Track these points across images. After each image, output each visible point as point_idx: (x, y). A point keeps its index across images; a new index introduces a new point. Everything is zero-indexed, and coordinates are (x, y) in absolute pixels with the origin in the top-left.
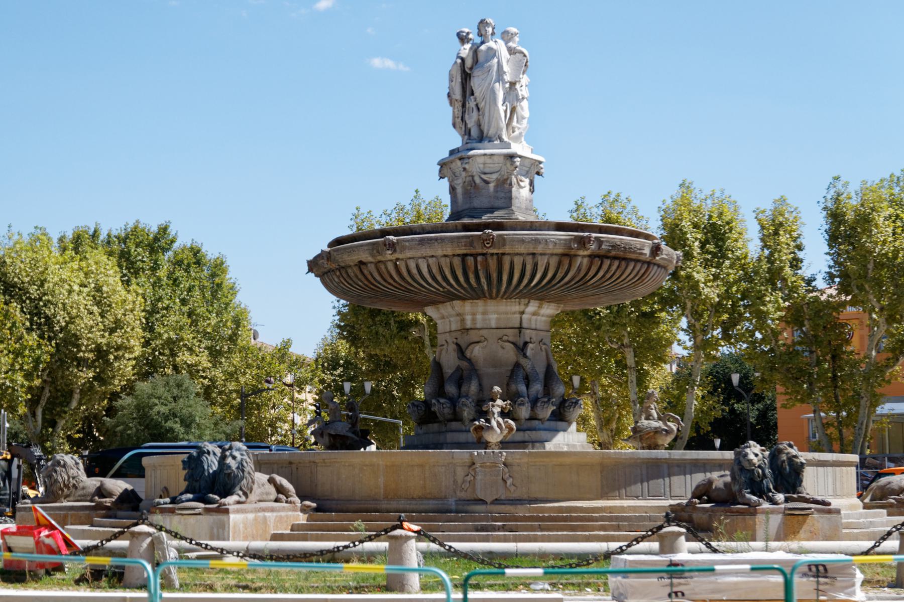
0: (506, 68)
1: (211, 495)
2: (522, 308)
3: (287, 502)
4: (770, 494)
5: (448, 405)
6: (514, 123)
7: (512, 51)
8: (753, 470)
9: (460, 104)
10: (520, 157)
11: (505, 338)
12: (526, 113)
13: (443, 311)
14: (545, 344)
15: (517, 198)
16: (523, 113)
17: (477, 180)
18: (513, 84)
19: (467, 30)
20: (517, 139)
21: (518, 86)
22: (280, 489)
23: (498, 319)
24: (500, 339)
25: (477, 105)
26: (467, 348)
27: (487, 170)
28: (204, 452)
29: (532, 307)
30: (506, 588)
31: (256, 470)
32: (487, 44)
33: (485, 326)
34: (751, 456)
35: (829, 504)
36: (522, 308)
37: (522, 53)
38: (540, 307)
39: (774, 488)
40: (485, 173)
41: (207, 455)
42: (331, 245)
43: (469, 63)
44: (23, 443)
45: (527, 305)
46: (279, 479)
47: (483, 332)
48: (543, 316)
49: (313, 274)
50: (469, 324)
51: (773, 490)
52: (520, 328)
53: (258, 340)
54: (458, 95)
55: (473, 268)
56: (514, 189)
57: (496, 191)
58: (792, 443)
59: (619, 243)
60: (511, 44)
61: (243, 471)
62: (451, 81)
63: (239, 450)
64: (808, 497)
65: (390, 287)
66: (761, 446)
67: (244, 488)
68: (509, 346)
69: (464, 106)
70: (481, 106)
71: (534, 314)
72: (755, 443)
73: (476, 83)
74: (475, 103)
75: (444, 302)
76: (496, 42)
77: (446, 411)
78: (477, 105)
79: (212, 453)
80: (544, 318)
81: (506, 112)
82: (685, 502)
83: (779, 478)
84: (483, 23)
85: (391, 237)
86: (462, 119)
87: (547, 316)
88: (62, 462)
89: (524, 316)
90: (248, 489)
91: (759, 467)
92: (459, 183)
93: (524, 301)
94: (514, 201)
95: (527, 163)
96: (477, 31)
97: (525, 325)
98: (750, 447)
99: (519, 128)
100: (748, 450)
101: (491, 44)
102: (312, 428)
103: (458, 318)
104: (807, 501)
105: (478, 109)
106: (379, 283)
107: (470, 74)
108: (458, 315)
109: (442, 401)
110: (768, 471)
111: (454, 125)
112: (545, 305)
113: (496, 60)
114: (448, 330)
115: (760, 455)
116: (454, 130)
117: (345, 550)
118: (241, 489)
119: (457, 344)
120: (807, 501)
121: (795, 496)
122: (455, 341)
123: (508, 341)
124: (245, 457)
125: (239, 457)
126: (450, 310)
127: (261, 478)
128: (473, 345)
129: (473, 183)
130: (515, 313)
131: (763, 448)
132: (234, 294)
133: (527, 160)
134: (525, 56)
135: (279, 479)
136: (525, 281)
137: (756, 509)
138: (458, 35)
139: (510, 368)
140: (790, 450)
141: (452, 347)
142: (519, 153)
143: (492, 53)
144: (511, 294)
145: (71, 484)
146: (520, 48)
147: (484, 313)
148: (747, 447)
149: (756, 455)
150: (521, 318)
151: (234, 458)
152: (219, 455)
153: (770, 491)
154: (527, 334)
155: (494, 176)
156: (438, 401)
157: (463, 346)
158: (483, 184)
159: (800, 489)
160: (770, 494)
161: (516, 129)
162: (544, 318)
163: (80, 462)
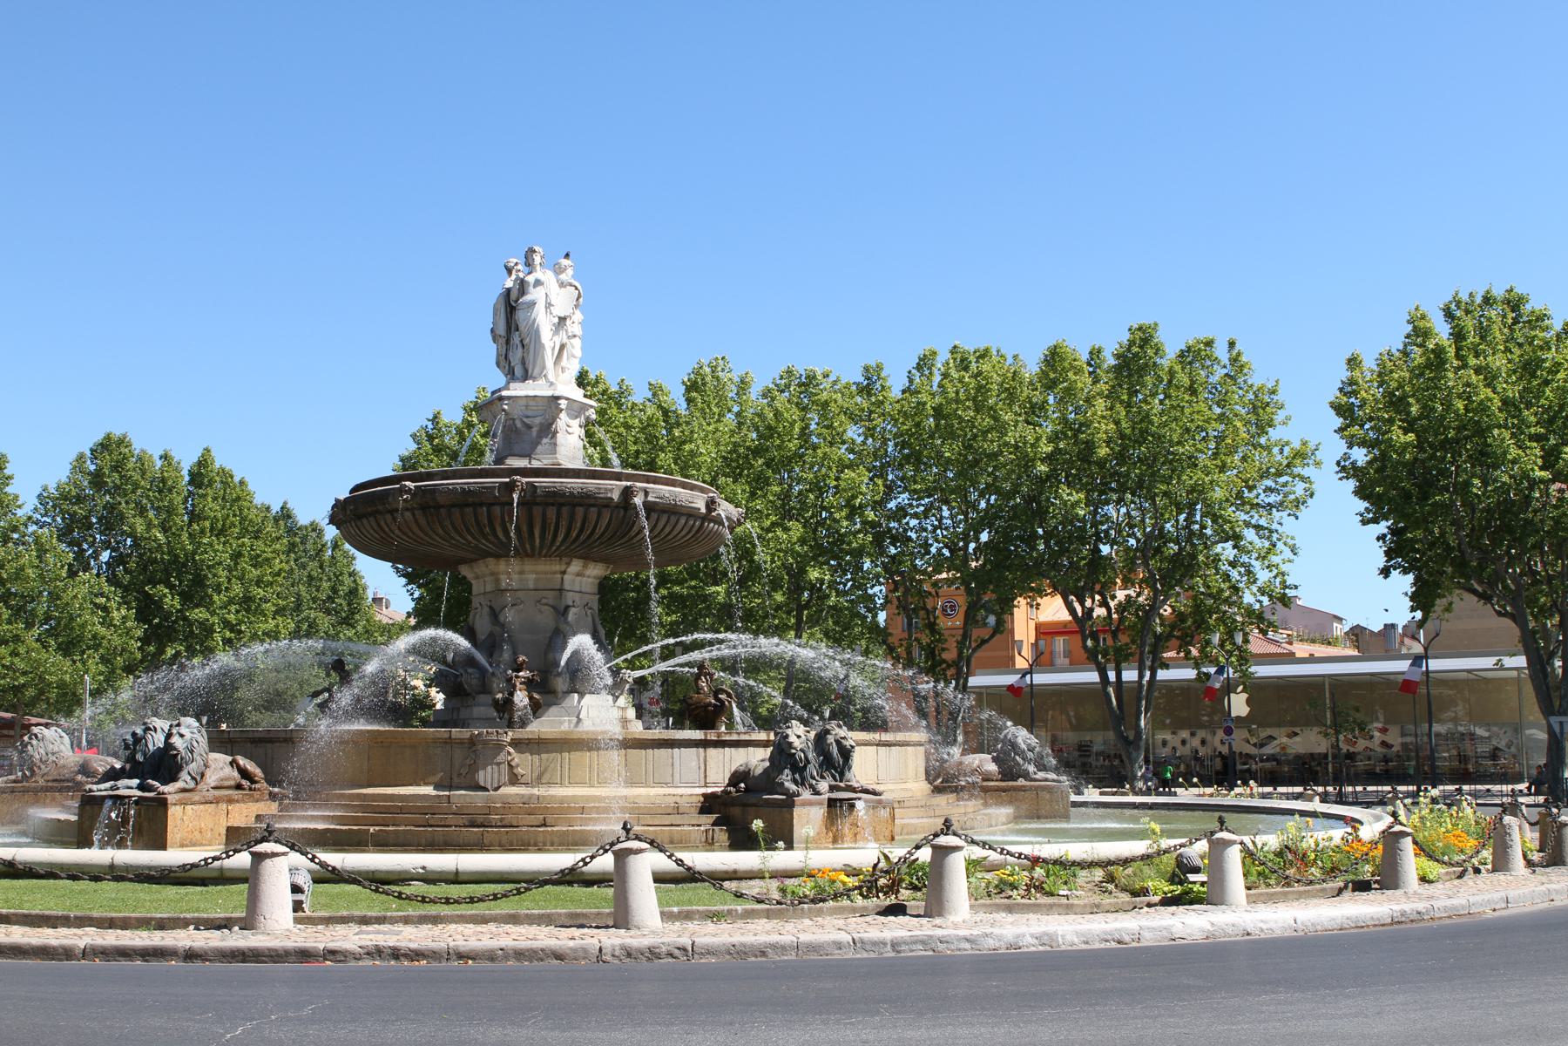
1: (150, 781)
3: (250, 789)
4: (814, 782)
5: (477, 676)
8: (795, 754)
9: (504, 340)
10: (567, 399)
11: (544, 601)
13: (476, 570)
14: (590, 608)
17: (519, 424)
18: (562, 320)
21: (568, 322)
22: (244, 773)
23: (536, 580)
25: (521, 341)
27: (530, 413)
29: (576, 566)
31: (212, 750)
33: (522, 587)
34: (792, 739)
38: (585, 566)
40: (527, 417)
41: (153, 733)
42: (351, 492)
43: (514, 295)
45: (568, 564)
46: (242, 761)
47: (520, 594)
48: (589, 577)
52: (561, 590)
54: (502, 330)
55: (499, 520)
59: (667, 495)
60: (563, 277)
61: (192, 752)
62: (495, 314)
63: (189, 727)
64: (856, 785)
65: (405, 537)
66: (805, 726)
68: (547, 610)
69: (508, 342)
70: (525, 343)
71: (578, 575)
72: (798, 723)
73: (520, 315)
75: (476, 560)
77: (474, 682)
78: (521, 341)
79: (159, 730)
80: (590, 580)
81: (553, 349)
82: (720, 789)
85: (407, 483)
86: (506, 358)
87: (595, 577)
89: (566, 577)
91: (802, 750)
93: (565, 560)
94: (558, 448)
95: (575, 405)
97: (567, 587)
100: (789, 731)
102: (63, 721)
103: (492, 578)
104: (854, 790)
105: (523, 346)
108: (492, 574)
109: (470, 670)
110: (811, 756)
111: (498, 364)
112: (591, 566)
115: (803, 737)
119: (491, 607)
120: (854, 790)
121: (842, 785)
123: (546, 604)
124: (197, 736)
125: (188, 736)
126: (484, 569)
127: (220, 760)
130: (555, 573)
132: (1412, 606)
133: (575, 404)
134: (576, 289)
135: (242, 761)
138: (506, 267)
139: (549, 635)
140: (837, 730)
141: (486, 610)
144: (550, 548)
147: (521, 573)
148: (788, 727)
149: (799, 737)
151: (182, 736)
153: (813, 778)
154: (569, 598)
155: (538, 421)
156: (466, 671)
158: (524, 429)
159: (848, 775)
162: (590, 580)
163: (63, 734)
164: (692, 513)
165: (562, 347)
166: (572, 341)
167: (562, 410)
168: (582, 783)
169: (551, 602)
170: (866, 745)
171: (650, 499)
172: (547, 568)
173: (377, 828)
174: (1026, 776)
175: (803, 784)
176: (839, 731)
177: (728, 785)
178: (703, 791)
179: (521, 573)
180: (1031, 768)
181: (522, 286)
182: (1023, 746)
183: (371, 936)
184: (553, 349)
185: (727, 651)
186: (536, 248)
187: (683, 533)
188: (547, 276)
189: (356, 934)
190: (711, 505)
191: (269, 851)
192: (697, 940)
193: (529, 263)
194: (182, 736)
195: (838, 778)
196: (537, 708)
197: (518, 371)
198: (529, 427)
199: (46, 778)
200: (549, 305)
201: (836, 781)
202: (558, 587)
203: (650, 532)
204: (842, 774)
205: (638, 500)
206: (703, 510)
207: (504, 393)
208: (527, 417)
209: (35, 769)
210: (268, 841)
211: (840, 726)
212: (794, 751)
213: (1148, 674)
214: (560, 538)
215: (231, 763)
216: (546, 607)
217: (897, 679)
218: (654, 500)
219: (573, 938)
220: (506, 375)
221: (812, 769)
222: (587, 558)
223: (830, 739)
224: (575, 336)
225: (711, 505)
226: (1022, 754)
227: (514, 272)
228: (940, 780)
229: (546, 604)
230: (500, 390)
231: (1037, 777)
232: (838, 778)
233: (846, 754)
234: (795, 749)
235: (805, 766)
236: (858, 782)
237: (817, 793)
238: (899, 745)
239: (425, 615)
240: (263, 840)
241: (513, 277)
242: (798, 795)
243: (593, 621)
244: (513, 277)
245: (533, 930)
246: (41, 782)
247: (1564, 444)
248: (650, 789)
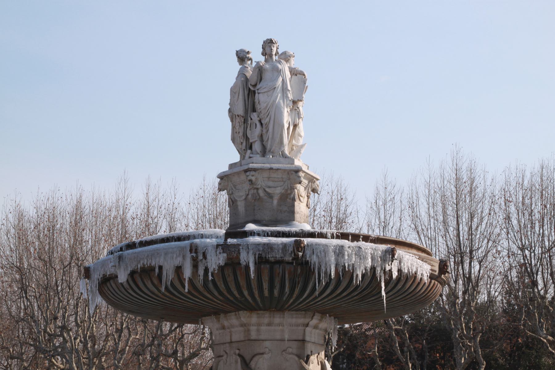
2: (306, 321)
11: (290, 350)
15: (298, 213)
24: (284, 351)
25: (260, 121)
26: (251, 360)
36: (306, 321)
40: (269, 187)
44: (535, 328)
50: (253, 335)
52: (303, 341)
54: (240, 111)
56: (296, 203)
57: (279, 205)
69: (245, 121)
73: (262, 99)
74: (258, 119)
84: (269, 43)
92: (240, 195)
96: (262, 50)
97: (307, 338)
105: (262, 124)
106: (160, 298)
107: (254, 92)
108: (243, 325)
111: (233, 140)
114: (229, 341)
116: (233, 144)
122: (237, 352)
123: (292, 354)
128: (257, 357)
129: (257, 198)
136: (328, 291)
138: (238, 53)
150: (304, 330)
157: (247, 358)
158: (266, 198)
169: (295, 351)
172: (294, 321)
179: (259, 325)
198: (270, 196)
200: (284, 89)
202: (301, 338)
208: (269, 187)
213: (470, 237)
214: (328, 291)
216: (291, 356)
229: (292, 354)
247: (121, 369)
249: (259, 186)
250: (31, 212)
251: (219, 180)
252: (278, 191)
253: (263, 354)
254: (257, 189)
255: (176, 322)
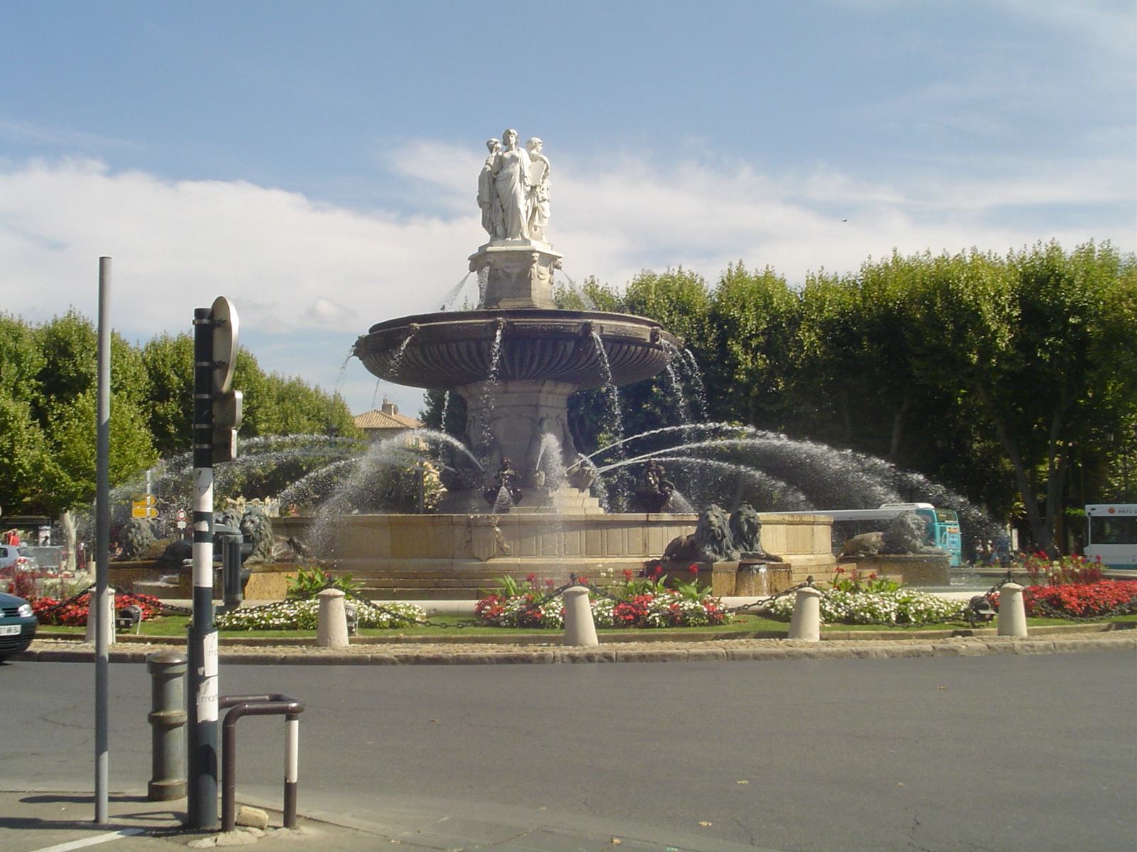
0: (527, 173)
4: (729, 551)
6: (536, 222)
7: (533, 158)
8: (713, 530)
12: (547, 213)
14: (561, 420)
16: (544, 214)
17: (501, 274)
18: (533, 188)
19: (495, 140)
20: (539, 238)
25: (502, 206)
28: (228, 517)
29: (548, 386)
30: (122, 633)
32: (511, 152)
34: (713, 519)
35: (780, 560)
37: (542, 160)
39: (733, 546)
40: (508, 268)
41: (231, 520)
45: (543, 384)
49: (358, 358)
51: (731, 548)
53: (398, 413)
54: (486, 199)
58: (750, 506)
60: (534, 152)
66: (722, 509)
67: (261, 549)
70: (504, 207)
73: (500, 185)
76: (518, 150)
78: (502, 206)
79: (235, 518)
81: (527, 212)
83: (738, 537)
85: (415, 324)
88: (137, 525)
90: (265, 550)
91: (720, 527)
98: (711, 509)
99: (540, 227)
100: (709, 513)
101: (514, 152)
105: (503, 210)
109: (466, 470)
113: (518, 167)
115: (721, 517)
117: (282, 601)
118: (259, 550)
131: (724, 511)
134: (545, 162)
137: (712, 566)
142: (537, 249)
143: (515, 159)
145: (145, 544)
146: (542, 156)
148: (709, 510)
149: (717, 517)
151: (252, 522)
152: (241, 519)
153: (728, 548)
156: (463, 470)
160: (729, 551)
161: (538, 228)
164: (638, 342)
165: (535, 209)
166: (542, 204)
167: (535, 262)
168: (545, 554)
170: (776, 524)
171: (604, 333)
173: (399, 589)
174: (914, 550)
175: (720, 554)
176: (748, 511)
177: (665, 555)
178: (645, 560)
180: (919, 543)
181: (501, 163)
182: (913, 526)
183: (402, 650)
184: (527, 212)
185: (1092, 375)
186: (512, 131)
187: (633, 359)
188: (522, 154)
189: (393, 648)
190: (654, 336)
191: (331, 594)
192: (619, 652)
193: (506, 142)
194: (252, 522)
195: (748, 548)
196: (517, 499)
197: (500, 230)
198: (509, 276)
199: (142, 557)
200: (522, 177)
201: (747, 550)
203: (608, 355)
204: (752, 546)
205: (595, 334)
206: (648, 340)
207: (489, 249)
208: (508, 268)
209: (135, 550)
210: (330, 587)
211: (749, 509)
212: (713, 528)
215: (289, 542)
217: (631, 482)
218: (607, 333)
219: (536, 651)
220: (490, 234)
221: (728, 541)
222: (558, 380)
223: (743, 519)
224: (544, 200)
225: (654, 336)
226: (911, 531)
227: (494, 150)
228: (842, 554)
230: (486, 246)
231: (922, 550)
232: (748, 548)
233: (754, 529)
234: (714, 526)
235: (722, 540)
236: (764, 551)
237: (730, 559)
238: (806, 524)
239: (431, 421)
240: (326, 587)
241: (494, 154)
242: (716, 561)
243: (564, 431)
244: (494, 154)
245: (510, 646)
246: (139, 561)
248: (604, 559)
249: (498, 267)
250: (324, 307)
251: (469, 262)
252: (516, 271)
253: (500, 418)
254: (497, 270)
255: (539, 441)
